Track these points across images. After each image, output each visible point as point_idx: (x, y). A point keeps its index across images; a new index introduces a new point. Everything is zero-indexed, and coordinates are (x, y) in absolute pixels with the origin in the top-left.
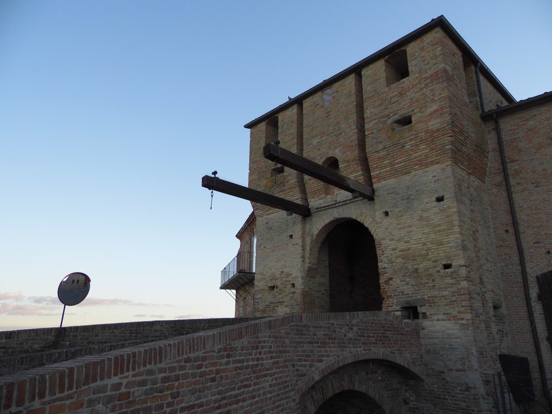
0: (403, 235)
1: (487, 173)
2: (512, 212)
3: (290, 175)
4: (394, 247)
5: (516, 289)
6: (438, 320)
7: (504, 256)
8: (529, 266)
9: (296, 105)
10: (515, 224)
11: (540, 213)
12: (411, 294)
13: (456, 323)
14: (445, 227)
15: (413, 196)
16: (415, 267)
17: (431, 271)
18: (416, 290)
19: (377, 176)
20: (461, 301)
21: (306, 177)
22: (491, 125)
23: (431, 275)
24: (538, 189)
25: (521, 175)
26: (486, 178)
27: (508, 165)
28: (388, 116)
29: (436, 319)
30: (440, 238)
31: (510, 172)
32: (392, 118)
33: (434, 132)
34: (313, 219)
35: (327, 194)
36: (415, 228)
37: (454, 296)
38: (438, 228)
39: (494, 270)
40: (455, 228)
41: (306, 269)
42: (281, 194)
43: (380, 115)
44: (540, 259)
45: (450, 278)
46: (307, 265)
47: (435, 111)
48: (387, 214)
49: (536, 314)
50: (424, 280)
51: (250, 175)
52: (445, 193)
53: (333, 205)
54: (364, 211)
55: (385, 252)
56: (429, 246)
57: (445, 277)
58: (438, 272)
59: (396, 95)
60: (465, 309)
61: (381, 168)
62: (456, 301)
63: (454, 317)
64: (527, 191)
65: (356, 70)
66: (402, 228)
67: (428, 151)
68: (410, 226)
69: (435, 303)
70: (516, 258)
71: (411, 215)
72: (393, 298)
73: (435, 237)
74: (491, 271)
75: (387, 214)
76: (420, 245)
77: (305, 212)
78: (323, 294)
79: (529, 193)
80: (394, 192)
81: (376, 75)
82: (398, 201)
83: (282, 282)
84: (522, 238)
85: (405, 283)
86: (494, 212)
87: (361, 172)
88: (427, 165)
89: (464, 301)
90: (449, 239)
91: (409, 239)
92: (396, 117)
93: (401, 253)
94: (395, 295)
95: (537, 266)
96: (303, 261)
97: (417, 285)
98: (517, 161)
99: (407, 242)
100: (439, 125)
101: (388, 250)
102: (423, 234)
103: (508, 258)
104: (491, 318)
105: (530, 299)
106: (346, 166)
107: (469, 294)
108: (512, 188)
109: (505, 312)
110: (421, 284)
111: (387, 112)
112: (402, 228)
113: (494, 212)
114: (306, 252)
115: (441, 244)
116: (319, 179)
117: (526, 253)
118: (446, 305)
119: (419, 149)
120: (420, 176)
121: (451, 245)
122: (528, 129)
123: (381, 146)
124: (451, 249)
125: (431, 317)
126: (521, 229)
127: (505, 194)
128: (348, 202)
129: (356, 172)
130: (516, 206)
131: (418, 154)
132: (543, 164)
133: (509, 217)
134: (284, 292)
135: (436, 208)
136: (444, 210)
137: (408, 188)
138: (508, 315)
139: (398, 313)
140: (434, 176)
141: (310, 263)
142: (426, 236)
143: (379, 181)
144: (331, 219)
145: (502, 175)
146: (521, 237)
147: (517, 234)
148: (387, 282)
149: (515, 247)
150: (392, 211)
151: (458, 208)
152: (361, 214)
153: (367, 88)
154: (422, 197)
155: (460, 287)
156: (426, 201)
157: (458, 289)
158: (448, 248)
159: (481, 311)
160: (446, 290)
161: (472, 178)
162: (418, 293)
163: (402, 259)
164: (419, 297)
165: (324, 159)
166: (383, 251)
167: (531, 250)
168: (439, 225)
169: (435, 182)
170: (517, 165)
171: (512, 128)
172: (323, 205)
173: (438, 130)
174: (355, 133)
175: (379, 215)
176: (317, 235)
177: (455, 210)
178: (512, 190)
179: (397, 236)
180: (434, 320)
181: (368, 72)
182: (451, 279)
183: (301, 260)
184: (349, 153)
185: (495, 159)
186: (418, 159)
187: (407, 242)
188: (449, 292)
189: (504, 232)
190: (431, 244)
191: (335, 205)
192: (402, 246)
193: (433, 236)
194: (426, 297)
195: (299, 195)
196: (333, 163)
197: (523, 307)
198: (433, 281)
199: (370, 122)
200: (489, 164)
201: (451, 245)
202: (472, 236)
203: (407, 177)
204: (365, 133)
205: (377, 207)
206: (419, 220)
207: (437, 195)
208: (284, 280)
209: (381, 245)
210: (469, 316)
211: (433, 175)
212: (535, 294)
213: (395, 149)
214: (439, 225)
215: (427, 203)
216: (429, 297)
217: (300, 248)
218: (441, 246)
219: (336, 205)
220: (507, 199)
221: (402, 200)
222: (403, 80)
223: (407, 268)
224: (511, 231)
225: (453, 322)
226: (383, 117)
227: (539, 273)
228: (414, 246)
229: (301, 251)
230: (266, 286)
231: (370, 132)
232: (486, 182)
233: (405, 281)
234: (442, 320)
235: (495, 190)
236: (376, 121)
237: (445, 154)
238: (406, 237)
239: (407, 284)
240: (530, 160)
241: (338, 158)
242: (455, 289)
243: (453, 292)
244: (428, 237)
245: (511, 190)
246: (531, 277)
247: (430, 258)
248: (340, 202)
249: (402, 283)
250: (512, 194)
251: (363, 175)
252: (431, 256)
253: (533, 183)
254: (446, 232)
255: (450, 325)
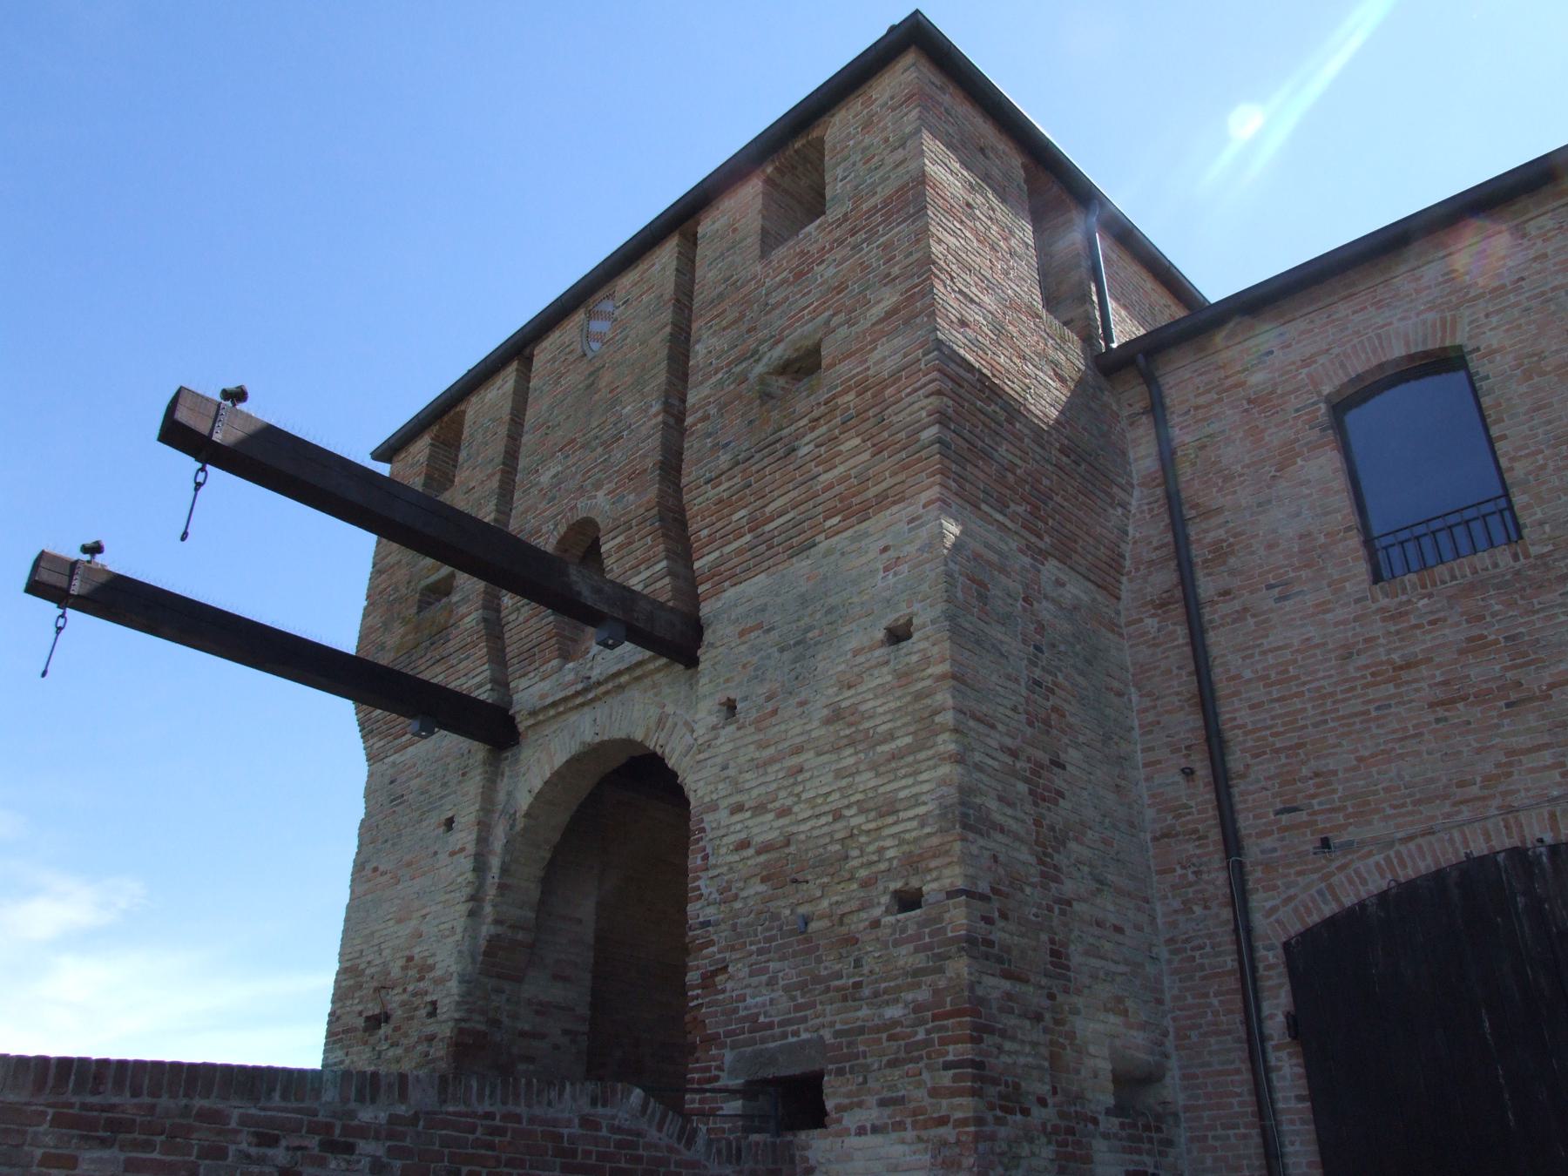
0: (774, 786)
1: (1128, 563)
2: (1206, 700)
3: (465, 600)
4: (743, 835)
5: (1215, 1002)
6: (861, 1131)
7: (1179, 871)
8: (1260, 901)
9: (515, 365)
10: (1215, 741)
11: (1296, 695)
12: (782, 1024)
13: (920, 1139)
14: (908, 740)
15: (817, 632)
16: (802, 910)
17: (858, 923)
18: (798, 1008)
19: (714, 572)
20: (943, 1042)
21: (508, 600)
22: (1134, 395)
23: (851, 941)
24: (1288, 605)
25: (1232, 561)
26: (1124, 579)
27: (1193, 531)
28: (756, 352)
29: (853, 1128)
30: (889, 788)
31: (1198, 553)
32: (765, 360)
33: (883, 385)
34: (522, 756)
35: (566, 656)
36: (811, 754)
37: (923, 1022)
38: (886, 748)
39: (1138, 928)
40: (940, 739)
41: (483, 943)
42: (438, 669)
43: (733, 355)
44: (1299, 873)
45: (911, 947)
46: (486, 929)
47: (890, 314)
48: (730, 707)
49: (1286, 1099)
50: (830, 965)
51: (367, 614)
52: (916, 607)
53: (577, 694)
54: (670, 709)
55: (712, 861)
56: (854, 822)
57: (896, 944)
58: (876, 924)
59: (784, 281)
60: (955, 1078)
61: (726, 539)
62: (927, 1043)
63: (915, 1113)
64: (1253, 616)
65: (682, 219)
66: (772, 761)
67: (866, 456)
68: (798, 750)
69: (857, 1056)
70: (1217, 878)
71: (802, 704)
72: (723, 1046)
73: (872, 783)
74: (1118, 929)
75: (730, 707)
76: (823, 820)
77: (495, 728)
78: (556, 1047)
79: (1256, 624)
80: (759, 626)
81: (735, 230)
82: (769, 657)
83: (405, 997)
84: (1237, 798)
85: (764, 978)
86: (1147, 702)
87: (664, 563)
88: (864, 513)
89: (955, 1041)
90: (914, 790)
91: (789, 802)
92: (779, 352)
93: (762, 858)
94: (728, 1034)
95: (1288, 906)
96: (472, 914)
97: (802, 986)
98: (1219, 510)
99: (784, 812)
100: (898, 357)
101: (723, 850)
102: (839, 775)
103: (1191, 877)
104: (1095, 1121)
105: (1263, 1039)
106: (620, 547)
107: (975, 1013)
108: (1206, 610)
109: (1181, 1099)
110: (817, 980)
111: (751, 343)
112: (772, 761)
113: (1147, 702)
114: (490, 881)
115: (889, 808)
116: (540, 602)
117: (1253, 851)
118: (893, 1064)
119: (840, 453)
120: (843, 554)
121: (922, 810)
122: (1250, 401)
123: (724, 459)
124: (923, 826)
125: (839, 1121)
126: (1236, 760)
127: (1181, 632)
128: (624, 679)
129: (648, 562)
130: (1218, 674)
131: (836, 472)
132: (1298, 515)
133: (1196, 720)
134: (406, 1035)
135: (885, 670)
136: (906, 674)
137: (804, 601)
138: (1187, 1109)
139: (734, 1106)
140: (885, 549)
141: (497, 922)
142: (844, 783)
143: (717, 592)
144: (573, 748)
145: (1173, 564)
146: (1235, 791)
147: (1222, 781)
148: (708, 980)
149: (1215, 835)
150: (745, 699)
151: (954, 661)
152: (661, 723)
153: (708, 275)
154: (847, 629)
155: (942, 984)
156: (854, 644)
157: (936, 992)
158: (915, 823)
159: (1044, 1089)
160: (896, 1001)
161: (1051, 568)
162: (804, 1020)
163: (763, 881)
164: (804, 1036)
165: (562, 529)
166: (706, 858)
167: (1268, 843)
168: (891, 736)
169: (886, 569)
170: (1219, 526)
171: (1201, 400)
172: (549, 700)
173: (895, 376)
174: (656, 425)
175: (706, 714)
176: (527, 815)
177: (944, 668)
178: (1207, 618)
179: (755, 793)
180: (846, 1132)
181: (717, 225)
182: (917, 950)
183: (463, 909)
184: (632, 497)
185: (1151, 510)
186: (837, 490)
187: (784, 812)
188: (906, 1005)
189: (1180, 778)
190: (861, 811)
191: (587, 694)
192: (766, 829)
193: (867, 779)
194: (827, 1034)
195: (485, 672)
196: (585, 540)
197: (1238, 1071)
198: (858, 963)
199: (701, 383)
200: (1131, 530)
201: (922, 810)
202: (1026, 781)
203: (802, 565)
204: (683, 421)
205: (704, 683)
206: (828, 722)
207: (889, 619)
208: (410, 988)
209: (703, 830)
210: (964, 1107)
211: (882, 544)
212: (1281, 1018)
213: (766, 462)
214: (891, 736)
215: (856, 653)
216: (837, 1034)
217: (466, 863)
218: (890, 820)
219: (590, 696)
220: (1188, 650)
221: (782, 650)
222: (807, 229)
223: (775, 917)
224: (1202, 770)
225: (910, 1134)
226: (740, 360)
227: (1296, 928)
228: (803, 828)
229: (470, 876)
230: (360, 1014)
231: (700, 414)
232: (1124, 595)
233: (764, 971)
234: (875, 1130)
235: (1151, 624)
236: (720, 375)
237: (920, 460)
238: (782, 794)
239: (771, 983)
240: (1259, 505)
241: (598, 520)
242: (923, 995)
243: (918, 1008)
244: (850, 786)
245: (1200, 616)
246: (1270, 948)
247: (852, 872)
248: (599, 684)
249: (754, 981)
250: (1203, 631)
251: (670, 572)
252: (855, 863)
253: (1270, 587)
254: (910, 759)
255: (901, 1148)
